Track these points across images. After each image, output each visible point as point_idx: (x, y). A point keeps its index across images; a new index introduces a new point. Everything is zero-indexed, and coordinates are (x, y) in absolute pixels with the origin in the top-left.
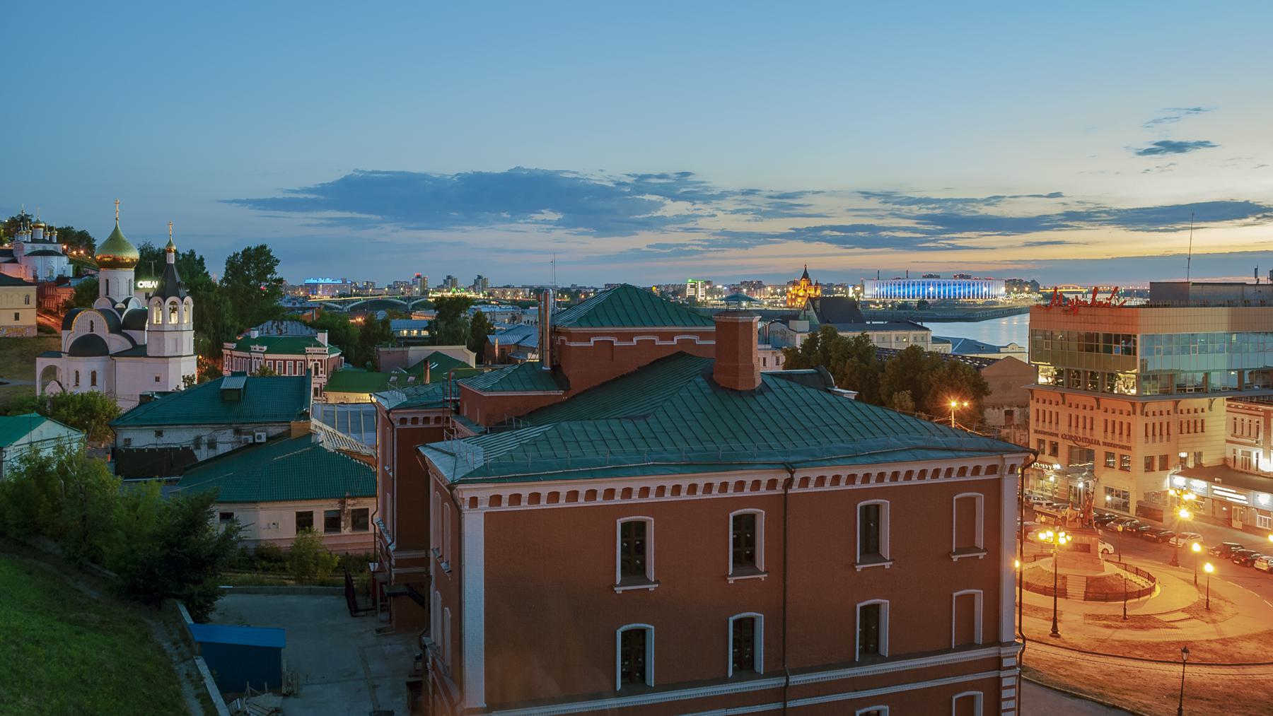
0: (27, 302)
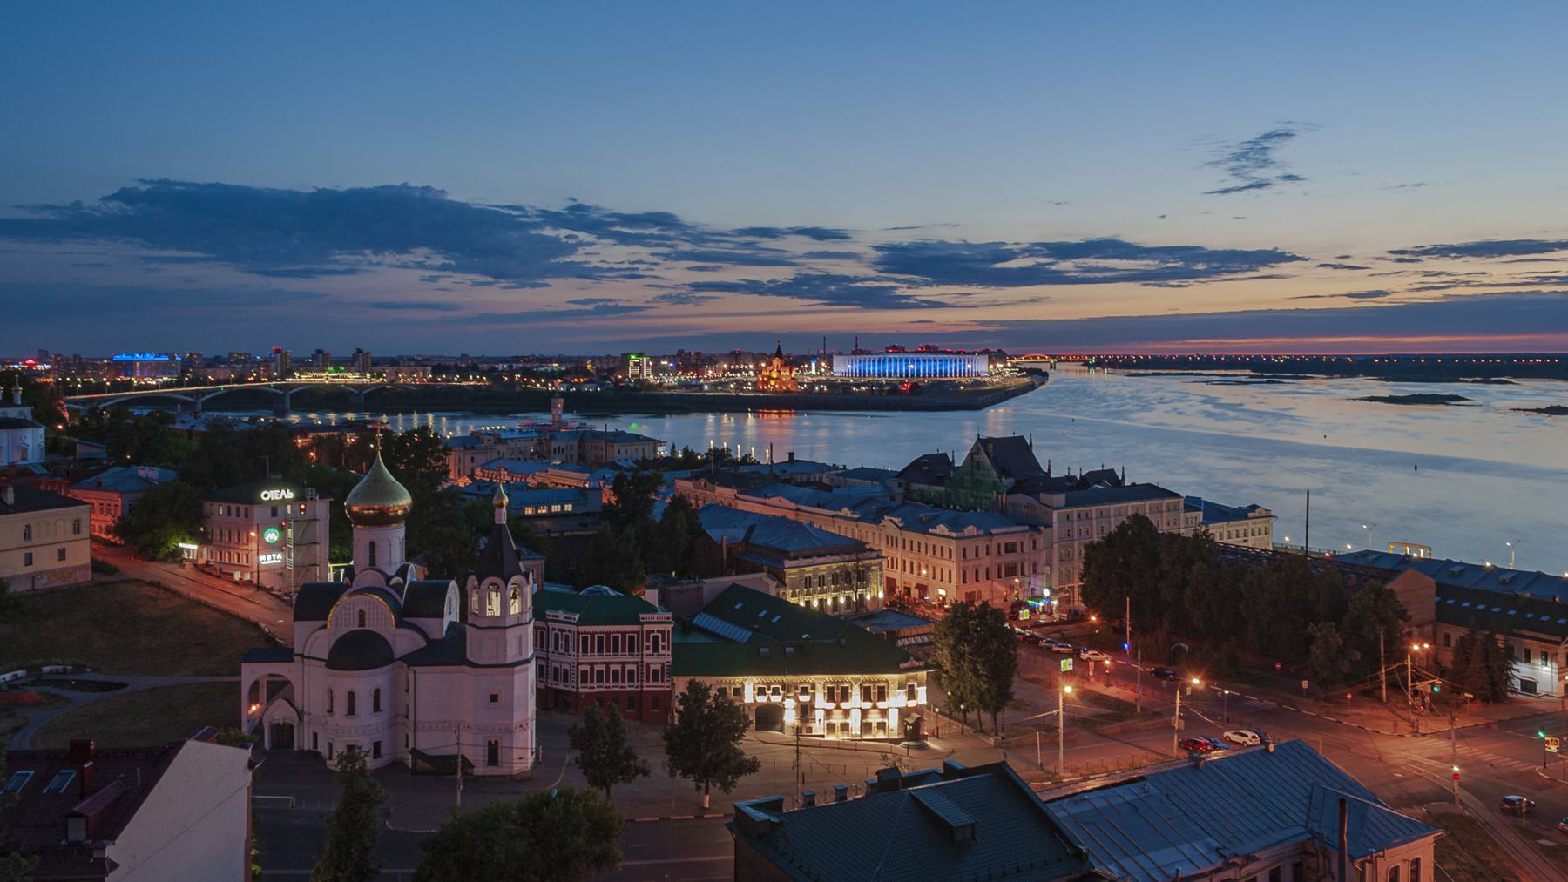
0: (77, 530)
